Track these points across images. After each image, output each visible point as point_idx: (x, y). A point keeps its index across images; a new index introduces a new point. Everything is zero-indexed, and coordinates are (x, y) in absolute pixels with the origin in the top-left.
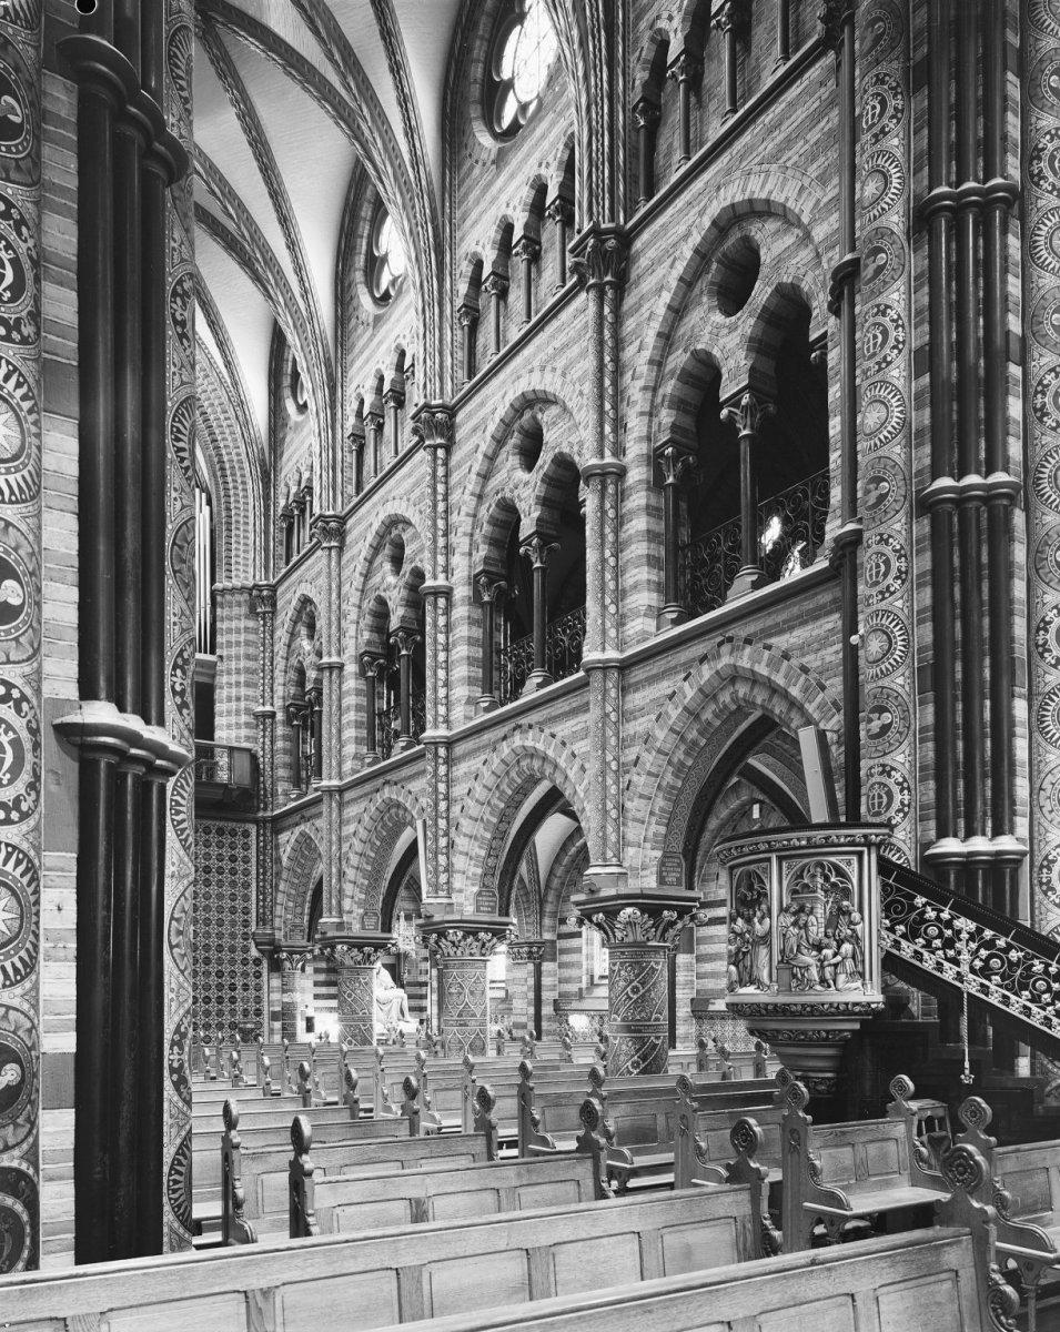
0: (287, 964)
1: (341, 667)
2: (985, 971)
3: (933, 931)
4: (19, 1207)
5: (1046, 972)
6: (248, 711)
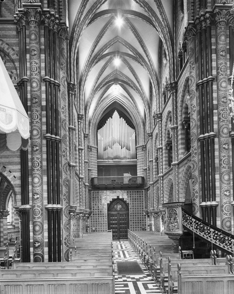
0: (150, 216)
1: (153, 161)
2: (197, 228)
3: (189, 221)
4: (40, 257)
5: (207, 229)
6: (142, 169)
